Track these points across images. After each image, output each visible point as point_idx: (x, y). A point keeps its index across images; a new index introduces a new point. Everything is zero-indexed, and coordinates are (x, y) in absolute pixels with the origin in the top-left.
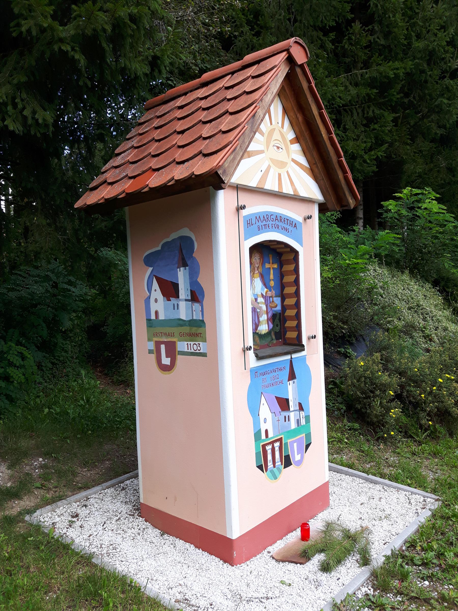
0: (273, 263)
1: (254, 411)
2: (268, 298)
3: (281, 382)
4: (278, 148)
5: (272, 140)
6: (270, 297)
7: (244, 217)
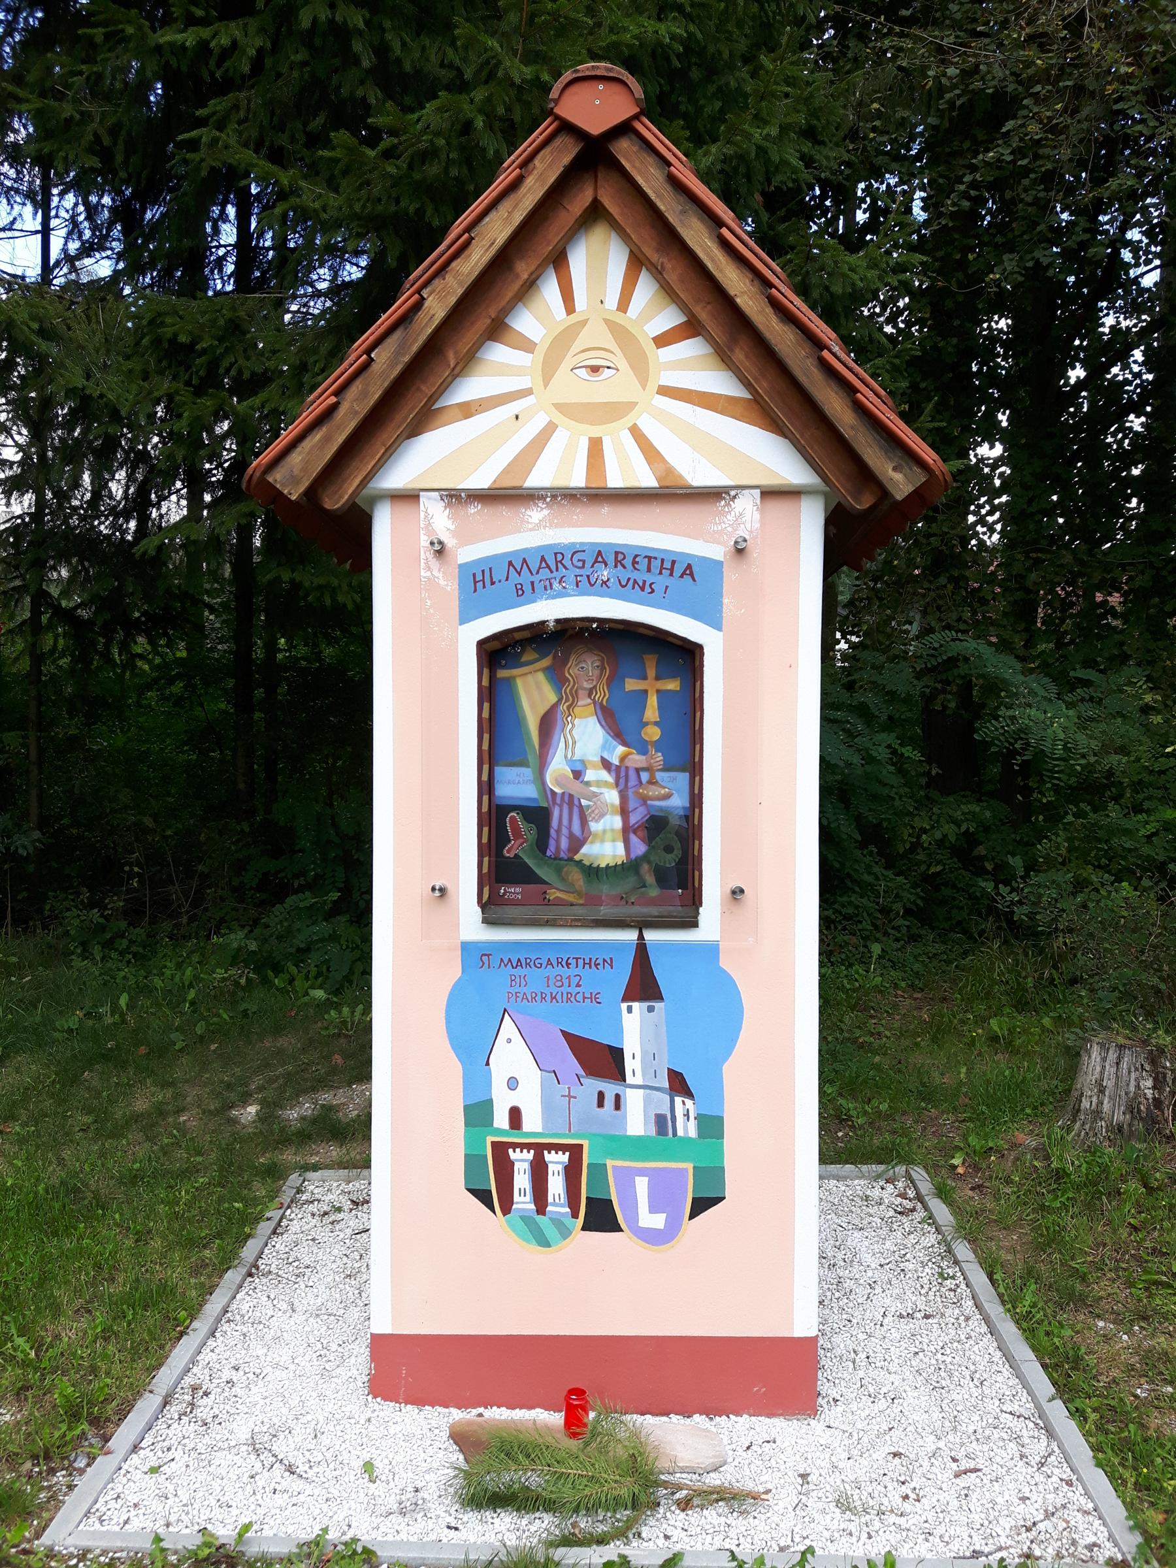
0: (658, 678)
1: (475, 1053)
2: (632, 774)
3: (594, 998)
4: (595, 369)
5: (575, 348)
6: (638, 770)
7: (461, 566)
